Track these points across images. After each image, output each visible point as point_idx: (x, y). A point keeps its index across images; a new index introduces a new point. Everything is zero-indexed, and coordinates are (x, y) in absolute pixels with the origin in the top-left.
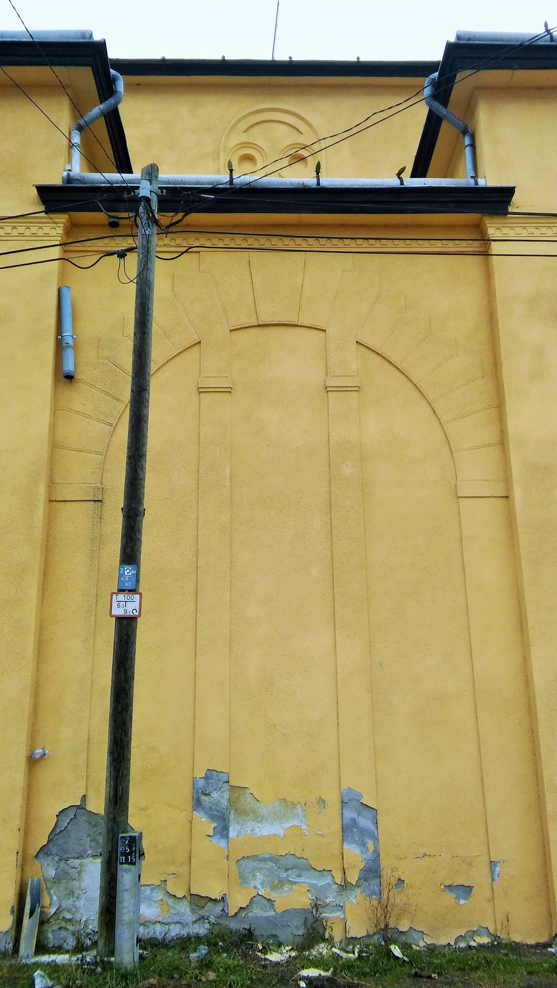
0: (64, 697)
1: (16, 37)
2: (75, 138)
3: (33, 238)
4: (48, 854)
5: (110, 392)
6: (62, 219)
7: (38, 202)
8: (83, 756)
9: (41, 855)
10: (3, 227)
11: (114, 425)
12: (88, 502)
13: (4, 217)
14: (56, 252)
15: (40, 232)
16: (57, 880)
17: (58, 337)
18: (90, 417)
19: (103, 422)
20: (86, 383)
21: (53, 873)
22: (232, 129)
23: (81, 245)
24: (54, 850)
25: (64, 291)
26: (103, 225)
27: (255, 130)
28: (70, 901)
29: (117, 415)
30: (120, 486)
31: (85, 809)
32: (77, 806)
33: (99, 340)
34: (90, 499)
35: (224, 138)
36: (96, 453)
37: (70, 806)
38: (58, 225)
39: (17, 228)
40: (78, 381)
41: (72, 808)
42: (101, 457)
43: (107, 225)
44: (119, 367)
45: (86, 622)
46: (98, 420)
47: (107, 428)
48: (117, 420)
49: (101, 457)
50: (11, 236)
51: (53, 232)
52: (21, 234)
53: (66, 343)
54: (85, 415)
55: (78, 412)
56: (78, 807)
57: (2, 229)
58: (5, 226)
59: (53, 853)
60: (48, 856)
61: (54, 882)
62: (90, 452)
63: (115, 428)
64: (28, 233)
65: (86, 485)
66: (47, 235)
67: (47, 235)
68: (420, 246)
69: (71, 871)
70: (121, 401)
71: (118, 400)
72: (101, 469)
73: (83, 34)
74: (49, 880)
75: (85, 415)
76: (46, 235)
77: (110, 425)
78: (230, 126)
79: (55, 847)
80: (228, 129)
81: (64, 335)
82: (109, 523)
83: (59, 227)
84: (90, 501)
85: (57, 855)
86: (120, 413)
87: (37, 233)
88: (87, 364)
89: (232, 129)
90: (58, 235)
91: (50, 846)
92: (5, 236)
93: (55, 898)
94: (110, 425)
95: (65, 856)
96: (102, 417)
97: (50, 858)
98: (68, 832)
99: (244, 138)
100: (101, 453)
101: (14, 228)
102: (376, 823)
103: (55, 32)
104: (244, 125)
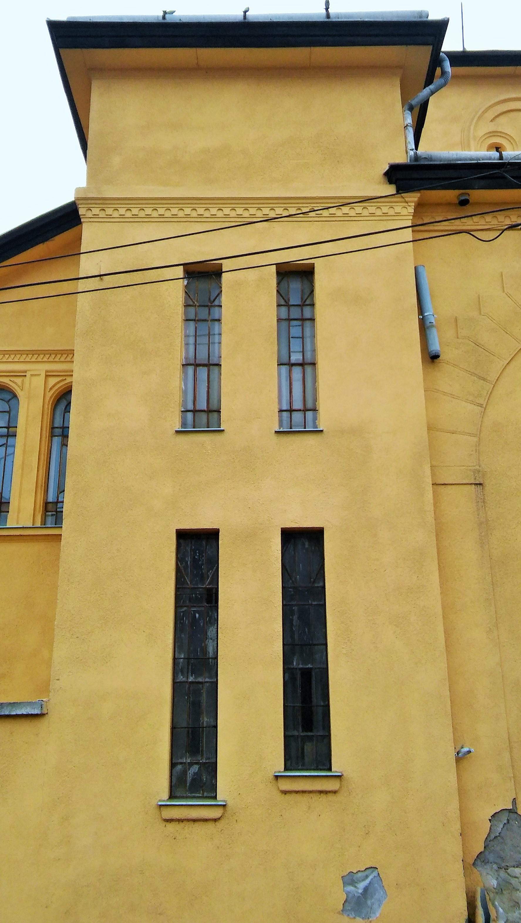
0: (475, 691)
1: (352, 17)
2: (408, 118)
3: (199, 220)
4: (486, 862)
5: (476, 372)
6: (413, 197)
7: (384, 182)
8: (506, 755)
9: (479, 862)
10: (288, 208)
11: (484, 406)
12: (469, 486)
13: (375, 197)
14: (408, 234)
15: (207, 214)
16: (500, 891)
17: (419, 317)
18: (458, 398)
19: (472, 403)
20: (448, 363)
21: (494, 883)
22: (480, 118)
23: (450, 224)
24: (491, 857)
25: (421, 270)
26: (455, 204)
27: (502, 120)
28: (517, 913)
29: (486, 396)
30: (498, 469)
31: (516, 813)
32: (509, 809)
33: (456, 320)
34: (471, 483)
35: (472, 127)
36: (470, 434)
37: (502, 810)
38: (409, 204)
39: (261, 210)
40: (442, 361)
41: (503, 812)
42: (476, 439)
43: (457, 203)
44: (481, 346)
45: (487, 611)
46: (467, 401)
47: (478, 409)
48: (486, 401)
49: (476, 439)
50: (336, 217)
51: (404, 212)
52: (372, 214)
53: (430, 323)
54: (452, 395)
55: (445, 394)
56: (510, 811)
57: (234, 211)
58: (224, 207)
59: (490, 861)
60: (485, 864)
61: (497, 893)
62: (463, 433)
63: (485, 409)
64: (142, 214)
65: (464, 467)
66: (386, 215)
67: (386, 215)
68: (476, 224)
69: (514, 881)
70: (488, 381)
71: (484, 379)
72: (478, 451)
73: (420, 14)
74: (491, 890)
75: (452, 395)
76: (398, 214)
77: (481, 405)
78: (478, 116)
79: (492, 855)
80: (475, 119)
81: (426, 314)
82: (493, 507)
83: (409, 206)
84: (471, 484)
85: (495, 863)
86: (489, 393)
87: (139, 215)
88: (448, 344)
89: (480, 118)
90: (409, 214)
91: (487, 853)
92: (356, 216)
93: (501, 910)
94: (481, 405)
95: (503, 865)
96: (471, 398)
97: (488, 866)
98: (502, 838)
99: (492, 127)
100: (475, 435)
101: (364, 208)
102: (63, 497)
103: (391, 13)
104: (490, 115)
